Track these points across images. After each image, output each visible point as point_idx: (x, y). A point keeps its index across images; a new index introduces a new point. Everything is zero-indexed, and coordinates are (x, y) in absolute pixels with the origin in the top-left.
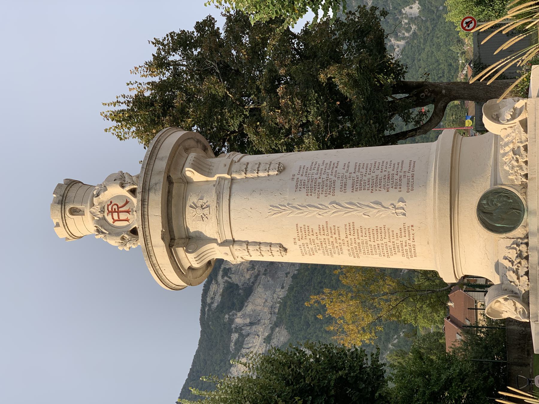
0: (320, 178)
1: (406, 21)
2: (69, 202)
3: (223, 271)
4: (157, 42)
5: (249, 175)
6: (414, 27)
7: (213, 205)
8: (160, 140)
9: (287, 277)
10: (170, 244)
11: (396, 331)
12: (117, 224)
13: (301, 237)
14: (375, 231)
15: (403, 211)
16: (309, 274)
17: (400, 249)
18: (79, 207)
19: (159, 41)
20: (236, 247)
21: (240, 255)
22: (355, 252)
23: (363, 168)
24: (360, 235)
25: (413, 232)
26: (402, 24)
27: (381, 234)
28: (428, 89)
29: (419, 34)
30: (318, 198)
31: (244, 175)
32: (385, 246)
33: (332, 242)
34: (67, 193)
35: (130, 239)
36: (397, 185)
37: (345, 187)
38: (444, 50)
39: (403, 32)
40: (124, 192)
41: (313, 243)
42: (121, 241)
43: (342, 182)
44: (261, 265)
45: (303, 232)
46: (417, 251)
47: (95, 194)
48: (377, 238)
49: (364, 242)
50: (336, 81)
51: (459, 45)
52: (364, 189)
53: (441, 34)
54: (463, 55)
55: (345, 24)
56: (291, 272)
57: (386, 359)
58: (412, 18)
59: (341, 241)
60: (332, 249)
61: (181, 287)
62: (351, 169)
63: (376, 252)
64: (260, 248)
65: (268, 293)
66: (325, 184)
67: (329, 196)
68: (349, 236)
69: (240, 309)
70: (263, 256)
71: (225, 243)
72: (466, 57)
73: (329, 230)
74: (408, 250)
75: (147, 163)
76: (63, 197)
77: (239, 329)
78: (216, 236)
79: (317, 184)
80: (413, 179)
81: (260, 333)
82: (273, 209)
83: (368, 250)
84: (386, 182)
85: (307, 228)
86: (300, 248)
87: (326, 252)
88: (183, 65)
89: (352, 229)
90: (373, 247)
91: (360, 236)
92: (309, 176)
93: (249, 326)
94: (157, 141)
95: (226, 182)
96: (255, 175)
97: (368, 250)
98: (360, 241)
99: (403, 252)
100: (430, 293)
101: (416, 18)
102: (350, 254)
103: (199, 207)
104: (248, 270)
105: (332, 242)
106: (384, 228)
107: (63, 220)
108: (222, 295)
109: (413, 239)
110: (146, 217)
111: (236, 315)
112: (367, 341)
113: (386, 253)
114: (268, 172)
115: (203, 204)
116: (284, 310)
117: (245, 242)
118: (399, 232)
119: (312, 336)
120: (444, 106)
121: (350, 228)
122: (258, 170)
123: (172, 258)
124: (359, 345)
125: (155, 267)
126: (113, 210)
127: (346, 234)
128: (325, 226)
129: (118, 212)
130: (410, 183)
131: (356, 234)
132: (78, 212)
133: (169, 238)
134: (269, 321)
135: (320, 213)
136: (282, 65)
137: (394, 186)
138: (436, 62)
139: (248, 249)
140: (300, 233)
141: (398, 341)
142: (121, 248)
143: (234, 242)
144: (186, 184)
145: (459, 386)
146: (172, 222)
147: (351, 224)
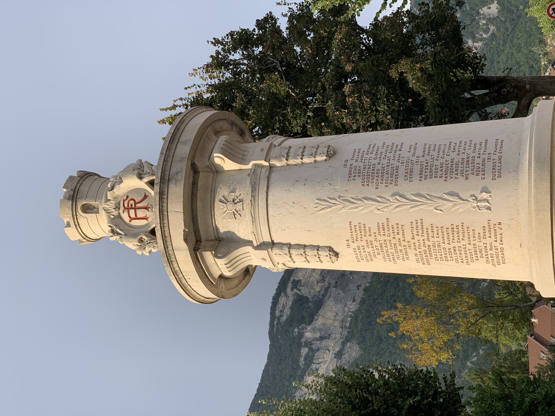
0: (379, 163)
1: (484, 22)
2: (81, 198)
3: (292, 283)
4: (216, 42)
5: (291, 162)
6: (492, 28)
7: (247, 199)
8: (184, 121)
9: (358, 289)
10: (195, 247)
11: (475, 348)
12: (135, 223)
13: (355, 239)
14: (450, 230)
15: (487, 204)
16: (381, 287)
17: (484, 253)
18: (93, 203)
19: (219, 41)
20: (276, 251)
21: (281, 262)
22: (424, 256)
23: (434, 150)
24: (431, 235)
25: (501, 232)
26: (480, 25)
27: (458, 233)
28: (510, 84)
29: (498, 35)
30: (376, 188)
31: (286, 161)
32: (463, 249)
33: (395, 244)
34: (80, 187)
35: (149, 241)
36: (480, 171)
37: (411, 175)
38: (525, 51)
39: (481, 33)
40: (142, 184)
41: (370, 246)
42: (139, 244)
43: (407, 168)
44: (331, 277)
45: (358, 232)
46: (506, 256)
47: (109, 187)
48: (453, 239)
49: (436, 245)
50: (409, 77)
51: (541, 46)
52: (436, 177)
53: (521, 34)
54: (545, 56)
55: (418, 17)
56: (362, 284)
57: (465, 378)
58: (490, 18)
59: (406, 243)
60: (395, 253)
61: (212, 300)
62: (419, 152)
63: (451, 257)
64: (304, 252)
65: (339, 306)
66: (385, 171)
67: (390, 186)
68: (416, 237)
69: (310, 323)
70: (309, 262)
71: (262, 246)
72: (549, 58)
73: (391, 229)
74: (495, 255)
75: (167, 148)
76: (74, 191)
77: (309, 344)
78: (251, 238)
79: (376, 172)
80: (500, 163)
81: (331, 348)
82: (321, 203)
83: (441, 255)
84: (465, 168)
85: (362, 226)
86: (355, 252)
87: (387, 258)
88: (243, 64)
89: (420, 227)
90: (448, 251)
91: (430, 237)
92: (366, 161)
93: (320, 340)
94: (180, 121)
95: (264, 170)
96: (299, 161)
97: (441, 255)
98: (431, 243)
99: (488, 258)
100: (513, 309)
101: (494, 19)
102: (417, 260)
103: (230, 201)
104: (318, 282)
105: (395, 244)
106: (462, 226)
107: (74, 219)
108: (292, 308)
109: (501, 241)
110: (165, 213)
111: (306, 328)
112: (444, 361)
113: (464, 259)
114: (315, 157)
115: (236, 198)
116: (356, 324)
117: (286, 244)
118: (481, 232)
119: (385, 352)
120: (528, 103)
121: (417, 227)
122: (303, 156)
123: (198, 264)
124: (435, 364)
125: (177, 275)
126: (130, 206)
127: (412, 234)
128: (386, 224)
129: (135, 209)
130: (497, 168)
131: (425, 234)
132: (92, 210)
133: (194, 240)
134: (340, 335)
135: (379, 208)
136: (349, 61)
137: (475, 171)
138: (516, 64)
139: (290, 254)
140: (354, 233)
141: (477, 359)
142: (139, 253)
143: (273, 244)
144: (216, 174)
145: (546, 411)
146: (197, 220)
147: (419, 222)
